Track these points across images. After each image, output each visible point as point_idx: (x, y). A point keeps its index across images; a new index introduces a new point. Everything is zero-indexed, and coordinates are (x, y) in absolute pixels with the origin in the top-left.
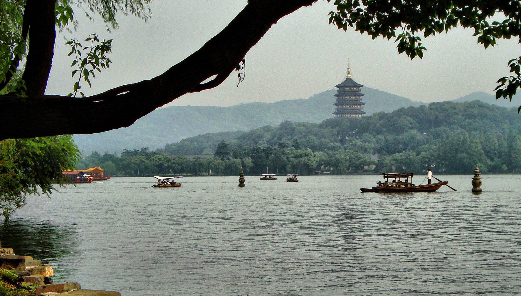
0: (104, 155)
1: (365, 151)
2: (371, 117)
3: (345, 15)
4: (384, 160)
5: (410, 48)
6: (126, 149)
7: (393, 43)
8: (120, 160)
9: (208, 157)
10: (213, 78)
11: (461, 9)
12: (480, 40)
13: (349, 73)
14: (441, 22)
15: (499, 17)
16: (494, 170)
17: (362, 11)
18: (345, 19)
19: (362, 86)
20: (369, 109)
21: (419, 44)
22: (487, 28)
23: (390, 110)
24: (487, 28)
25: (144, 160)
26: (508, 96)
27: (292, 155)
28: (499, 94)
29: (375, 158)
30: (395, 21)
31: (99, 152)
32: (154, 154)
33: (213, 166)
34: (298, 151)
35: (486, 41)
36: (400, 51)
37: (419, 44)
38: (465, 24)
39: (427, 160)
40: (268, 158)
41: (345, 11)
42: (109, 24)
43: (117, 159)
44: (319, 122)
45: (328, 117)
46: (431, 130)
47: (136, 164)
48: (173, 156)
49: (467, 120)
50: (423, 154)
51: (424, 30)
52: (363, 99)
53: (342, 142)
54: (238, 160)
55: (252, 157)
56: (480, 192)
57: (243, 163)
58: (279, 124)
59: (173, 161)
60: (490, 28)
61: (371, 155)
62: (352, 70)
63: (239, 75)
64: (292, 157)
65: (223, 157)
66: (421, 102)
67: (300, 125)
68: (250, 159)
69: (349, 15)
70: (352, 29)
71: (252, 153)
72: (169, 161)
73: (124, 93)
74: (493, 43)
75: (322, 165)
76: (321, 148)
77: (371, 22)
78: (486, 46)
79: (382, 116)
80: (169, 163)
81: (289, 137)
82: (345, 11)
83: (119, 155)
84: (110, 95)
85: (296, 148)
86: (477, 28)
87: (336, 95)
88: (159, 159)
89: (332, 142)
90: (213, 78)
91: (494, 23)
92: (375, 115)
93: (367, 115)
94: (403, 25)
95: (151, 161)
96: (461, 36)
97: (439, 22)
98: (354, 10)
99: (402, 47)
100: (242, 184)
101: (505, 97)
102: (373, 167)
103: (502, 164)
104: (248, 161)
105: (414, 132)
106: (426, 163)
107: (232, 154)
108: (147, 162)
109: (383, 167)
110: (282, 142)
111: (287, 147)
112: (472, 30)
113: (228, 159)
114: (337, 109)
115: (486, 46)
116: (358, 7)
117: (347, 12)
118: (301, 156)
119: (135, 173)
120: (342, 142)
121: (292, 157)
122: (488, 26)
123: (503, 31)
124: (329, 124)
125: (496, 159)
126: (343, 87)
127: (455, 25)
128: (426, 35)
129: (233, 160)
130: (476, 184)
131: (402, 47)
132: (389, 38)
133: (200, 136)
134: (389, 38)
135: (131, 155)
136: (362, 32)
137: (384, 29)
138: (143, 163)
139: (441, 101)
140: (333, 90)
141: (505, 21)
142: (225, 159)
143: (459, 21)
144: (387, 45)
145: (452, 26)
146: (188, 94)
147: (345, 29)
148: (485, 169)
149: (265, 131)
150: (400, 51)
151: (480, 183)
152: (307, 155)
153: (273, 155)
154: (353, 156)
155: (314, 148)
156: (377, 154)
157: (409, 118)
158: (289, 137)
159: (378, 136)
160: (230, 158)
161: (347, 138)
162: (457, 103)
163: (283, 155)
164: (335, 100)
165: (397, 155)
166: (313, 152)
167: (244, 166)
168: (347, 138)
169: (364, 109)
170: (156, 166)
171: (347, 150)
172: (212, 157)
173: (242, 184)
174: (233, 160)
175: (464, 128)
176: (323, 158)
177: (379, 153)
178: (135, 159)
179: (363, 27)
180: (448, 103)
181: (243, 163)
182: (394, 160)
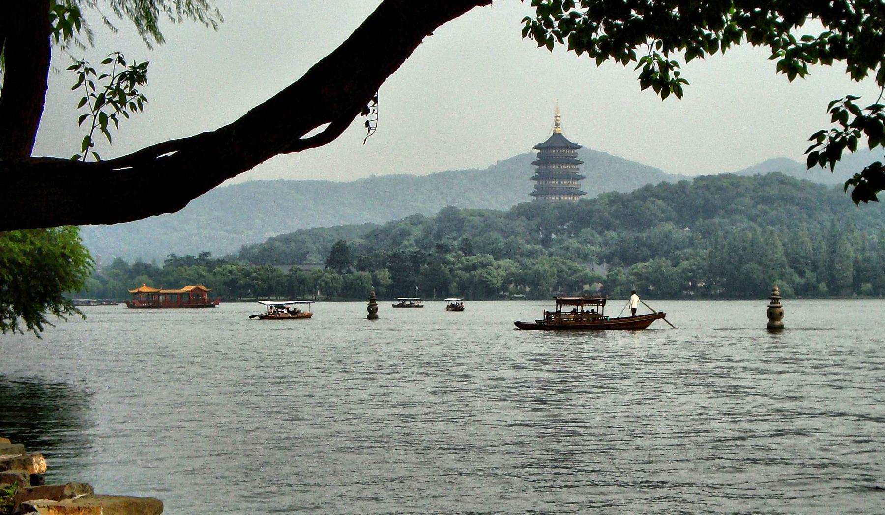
1: (585, 257)
2: (594, 201)
3: (549, 24)
4: (617, 274)
5: (659, 81)
7: (631, 72)
9: (317, 268)
10: (323, 128)
12: (781, 67)
13: (557, 125)
15: (813, 27)
16: (805, 292)
17: (578, 16)
18: (550, 30)
19: (580, 147)
21: (677, 74)
22: (793, 46)
23: (626, 188)
24: (793, 46)
25: (203, 273)
26: (828, 164)
27: (460, 265)
28: (813, 159)
29: (602, 271)
30: (636, 34)
32: (221, 262)
33: (323, 284)
35: (790, 69)
36: (644, 86)
38: (755, 39)
39: (690, 274)
40: (417, 271)
42: (150, 36)
44: (506, 209)
45: (521, 201)
50: (685, 264)
52: (582, 170)
54: (366, 274)
55: (390, 269)
56: (781, 328)
61: (595, 265)
63: (367, 124)
65: (341, 268)
67: (472, 213)
69: (556, 24)
70: (562, 48)
72: (247, 274)
73: (170, 154)
75: (511, 282)
77: (594, 36)
78: (791, 78)
79: (615, 199)
81: (455, 234)
83: (161, 265)
84: (146, 158)
85: (466, 254)
86: (775, 46)
87: (535, 163)
88: (231, 272)
89: (528, 243)
90: (323, 128)
92: (601, 197)
93: (588, 197)
94: (650, 40)
95: (215, 274)
98: (566, 15)
99: (647, 79)
100: (372, 315)
103: (818, 281)
104: (384, 275)
105: (669, 226)
106: (690, 279)
109: (616, 286)
112: (766, 50)
113: (349, 271)
115: (791, 78)
116: (572, 10)
117: (553, 19)
118: (475, 267)
121: (460, 269)
122: (795, 43)
123: (820, 52)
124: (523, 212)
125: (808, 273)
126: (547, 148)
127: (737, 42)
128: (689, 57)
129: (357, 273)
130: (774, 315)
131: (647, 79)
132: (625, 63)
133: (300, 232)
134: (625, 63)
135: (182, 265)
137: (617, 47)
140: (531, 154)
142: (344, 271)
143: (745, 34)
144: (620, 75)
145: (732, 43)
146: (280, 157)
147: (550, 47)
150: (644, 86)
151: (781, 313)
152: (484, 266)
157: (660, 202)
158: (455, 234)
160: (354, 270)
161: (553, 236)
162: (742, 178)
164: (533, 171)
165: (640, 265)
167: (376, 283)
168: (553, 236)
169: (584, 186)
170: (225, 283)
171: (554, 257)
172: (321, 268)
173: (372, 315)
174: (357, 273)
175: (754, 220)
176: (513, 270)
177: (608, 262)
179: (580, 43)
181: (374, 277)
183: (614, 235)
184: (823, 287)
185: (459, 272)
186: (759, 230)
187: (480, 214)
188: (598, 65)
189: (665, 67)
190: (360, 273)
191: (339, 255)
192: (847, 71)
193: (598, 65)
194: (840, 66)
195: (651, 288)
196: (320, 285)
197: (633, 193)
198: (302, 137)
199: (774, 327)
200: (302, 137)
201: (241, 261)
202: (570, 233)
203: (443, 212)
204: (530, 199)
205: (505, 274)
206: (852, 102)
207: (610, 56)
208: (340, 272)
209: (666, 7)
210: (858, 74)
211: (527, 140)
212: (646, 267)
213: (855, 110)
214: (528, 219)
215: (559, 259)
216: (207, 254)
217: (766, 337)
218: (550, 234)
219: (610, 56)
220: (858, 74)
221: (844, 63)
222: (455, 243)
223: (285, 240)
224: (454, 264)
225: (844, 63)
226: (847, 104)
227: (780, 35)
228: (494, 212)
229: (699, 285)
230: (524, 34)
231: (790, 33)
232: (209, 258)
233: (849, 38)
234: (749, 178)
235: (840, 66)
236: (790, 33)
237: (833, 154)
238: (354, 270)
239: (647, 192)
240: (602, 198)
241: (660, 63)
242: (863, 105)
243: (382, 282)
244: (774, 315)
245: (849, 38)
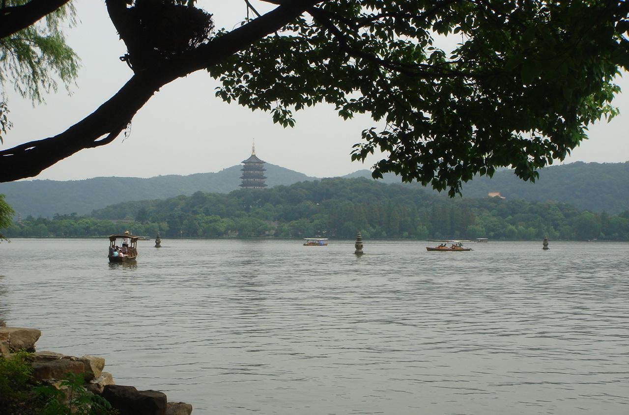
0: (38, 219)
1: (267, 218)
2: (272, 189)
3: (229, 90)
4: (282, 226)
5: (281, 118)
6: (57, 214)
7: (269, 115)
8: (52, 223)
9: (130, 221)
10: (106, 136)
11: (325, 89)
12: (341, 113)
13: (253, 151)
14: (309, 98)
15: (356, 95)
16: (376, 237)
17: (243, 87)
18: (229, 93)
19: (265, 162)
20: (271, 183)
21: (291, 116)
22: (346, 104)
23: (288, 183)
24: (346, 104)
25: (73, 223)
26: (361, 159)
27: (203, 221)
28: (355, 157)
29: (275, 225)
30: (272, 96)
31: (33, 216)
32: (82, 218)
33: (134, 229)
34: (209, 217)
35: (345, 114)
36: (275, 121)
37: (291, 116)
38: (329, 100)
39: (319, 227)
40: (182, 223)
41: (229, 86)
42: (36, 101)
43: (49, 222)
44: (227, 193)
45: (236, 189)
46: (323, 201)
47: (66, 227)
48: (99, 220)
49: (353, 194)
50: (316, 222)
51: (295, 104)
52: (265, 174)
53: (247, 210)
54: (156, 224)
55: (168, 222)
56: (362, 253)
57: (160, 227)
58: (193, 193)
59: (99, 224)
60: (348, 104)
61: (272, 222)
62: (256, 149)
63: (125, 133)
64: (203, 222)
65: (143, 221)
66: (315, 177)
67: (210, 195)
68: (167, 224)
69: (232, 90)
70: (235, 102)
71: (168, 219)
72: (95, 224)
73: (31, 148)
74: (351, 116)
75: (229, 229)
76: (228, 215)
77: (251, 97)
78: (345, 119)
79: (281, 189)
80: (95, 226)
81: (201, 205)
82: (229, 86)
83: (51, 219)
84: (19, 150)
85: (207, 215)
86: (338, 103)
87: (242, 170)
88: (87, 223)
89: (238, 210)
90: (106, 136)
91: (352, 100)
92: (275, 188)
93: (268, 187)
94: (279, 101)
95: (79, 224)
96: (325, 109)
97: (307, 98)
98: (237, 86)
99: (277, 118)
100: (158, 246)
101: (358, 160)
102: (273, 232)
103: (382, 231)
104: (165, 225)
105: (309, 203)
106: (319, 229)
107: (150, 219)
108: (76, 225)
109: (282, 232)
110: (194, 209)
111: (198, 214)
112: (334, 105)
113: (147, 223)
114: (243, 182)
115: (345, 119)
116: (240, 84)
117: (231, 88)
118: (211, 222)
119: (65, 235)
120: (247, 210)
121: (203, 222)
122: (347, 103)
123: (357, 107)
124: (235, 194)
125: (377, 227)
126: (248, 162)
127: (320, 101)
128: (297, 108)
129: (151, 224)
130: (359, 247)
131: (277, 118)
132: (265, 110)
133: (123, 203)
134: (265, 110)
135: (62, 219)
136: (244, 105)
137: (261, 103)
138: (72, 226)
139: (332, 176)
140: (240, 165)
141: (361, 99)
142: (144, 223)
143: (324, 97)
144: (264, 116)
145: (318, 102)
146: (85, 150)
147: (229, 101)
148: (368, 235)
149: (181, 200)
150: (275, 121)
151: (362, 246)
152: (216, 221)
153: (186, 221)
154: (256, 222)
155: (222, 215)
156: (276, 222)
157: (304, 190)
158: (201, 205)
159: (277, 205)
160: (149, 223)
161: (251, 207)
162: (345, 179)
163: (195, 221)
164: (241, 174)
165: (294, 222)
166: (222, 218)
167: (161, 230)
168: (251, 207)
169: (266, 182)
170: (84, 229)
171: (251, 218)
172: (133, 221)
173: (158, 246)
174: (151, 224)
175: (351, 200)
176: (231, 223)
177: (278, 220)
178: (65, 222)
179: (244, 101)
180: (338, 178)
181: (160, 227)
182: (291, 226)
183: (281, 206)
184: (384, 234)
185: (203, 224)
186: (353, 205)
187: (214, 195)
188: (253, 111)
189: (285, 112)
190: (153, 224)
191: (142, 215)
192: (372, 117)
193: (253, 111)
194: (368, 113)
195: (300, 233)
196: (132, 230)
197: (291, 186)
198: (96, 140)
199: (359, 253)
200: (96, 140)
201: (92, 217)
202: (259, 205)
203: (195, 194)
204: (239, 188)
205: (226, 225)
206: (373, 130)
207: (259, 108)
208: (142, 224)
209: (286, 84)
210: (377, 117)
211: (238, 159)
212: (297, 223)
213: (374, 134)
214: (239, 198)
215: (254, 218)
216: (75, 214)
217: (354, 258)
218: (249, 206)
219: (259, 108)
220: (377, 117)
221: (370, 112)
222: (201, 209)
223: (115, 207)
224: (200, 220)
225: (370, 112)
226: (370, 131)
227: (340, 98)
228: (221, 194)
229: (323, 232)
230: (217, 94)
231: (345, 97)
232: (76, 215)
233: (373, 100)
234: (349, 179)
235: (368, 113)
236: (345, 97)
237: (363, 155)
238: (149, 223)
239: (298, 186)
240: (276, 188)
241: (283, 111)
242: (378, 132)
243: (163, 229)
244: (359, 247)
245: (373, 100)
